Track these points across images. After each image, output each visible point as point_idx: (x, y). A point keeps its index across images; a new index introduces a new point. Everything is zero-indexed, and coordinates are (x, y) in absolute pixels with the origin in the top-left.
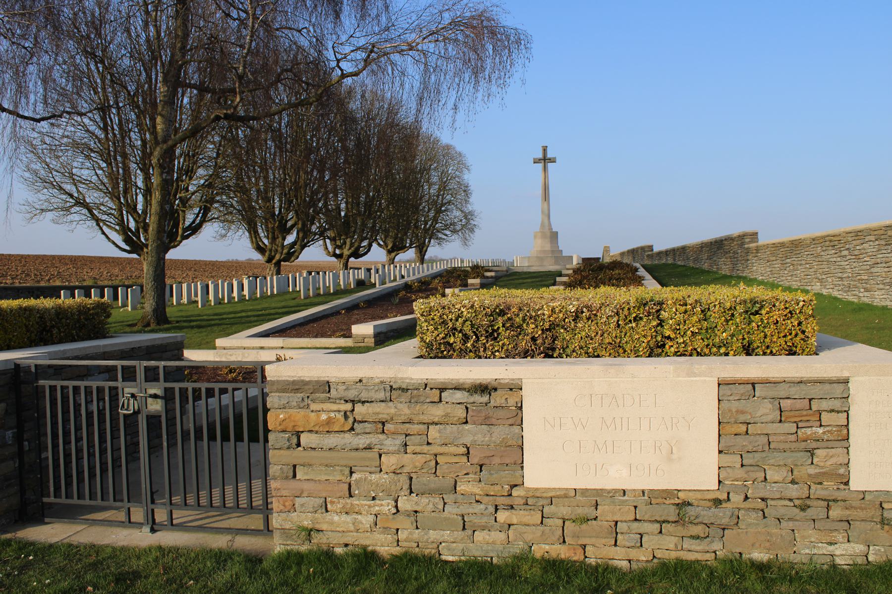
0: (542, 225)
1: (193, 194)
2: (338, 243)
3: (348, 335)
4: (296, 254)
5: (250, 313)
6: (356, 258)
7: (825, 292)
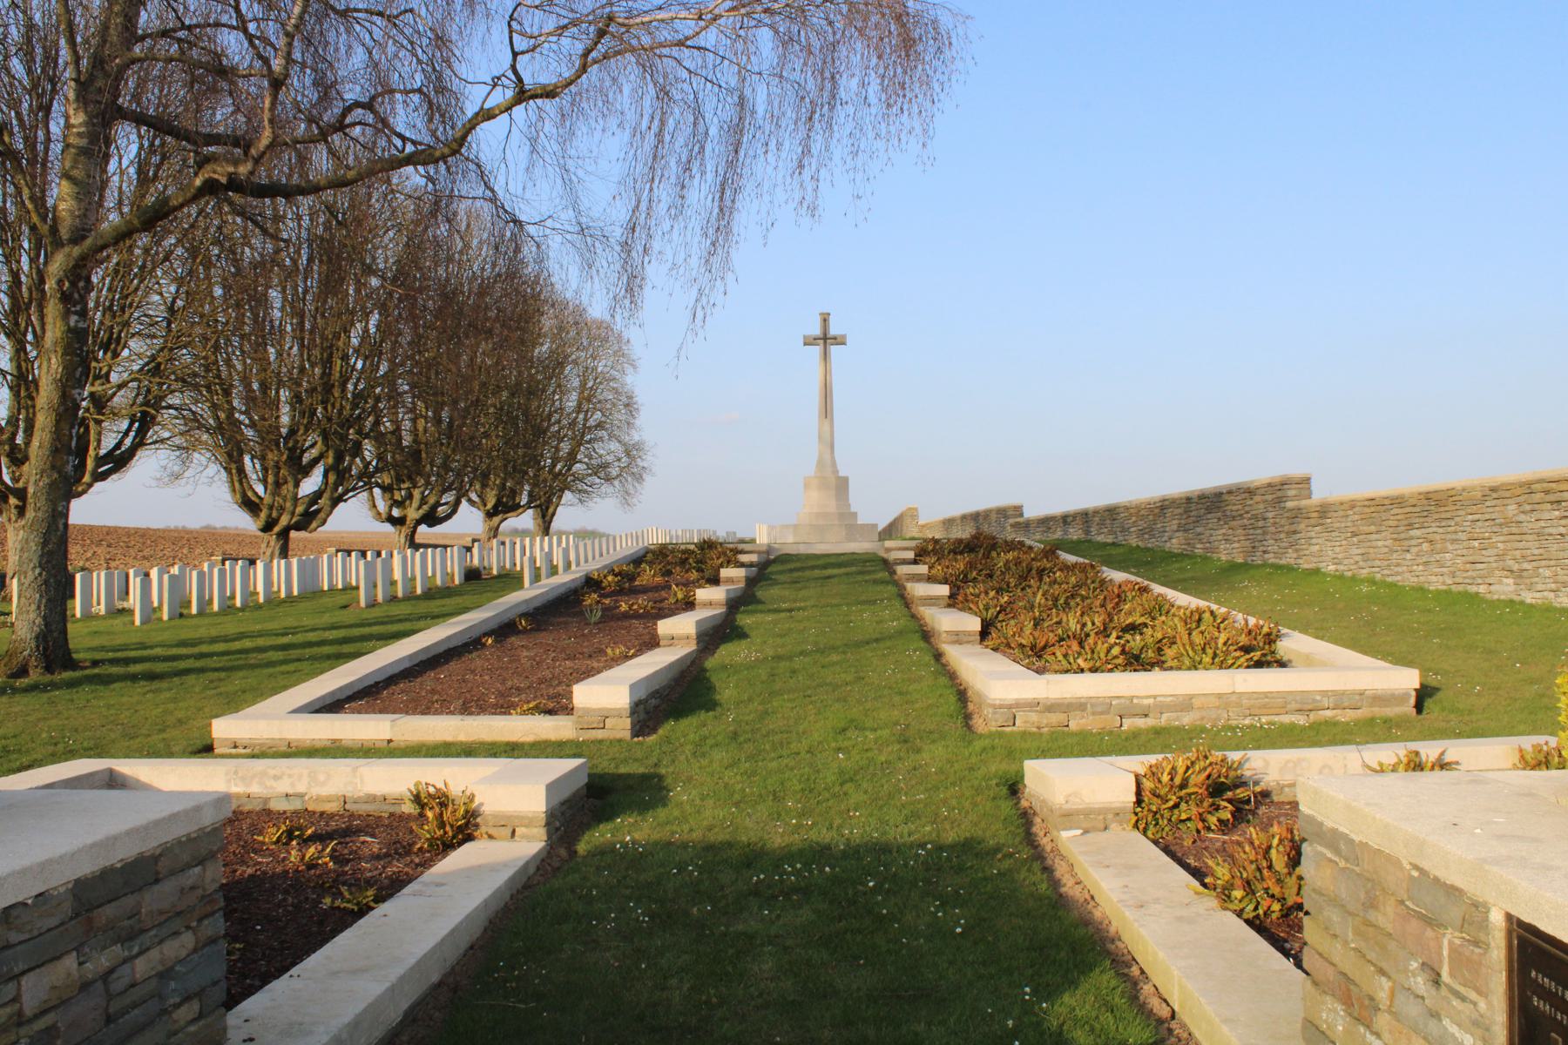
0: (820, 463)
1: (120, 387)
2: (397, 497)
3: (559, 706)
4: (322, 515)
5: (261, 642)
6: (430, 526)
7: (1529, 597)
